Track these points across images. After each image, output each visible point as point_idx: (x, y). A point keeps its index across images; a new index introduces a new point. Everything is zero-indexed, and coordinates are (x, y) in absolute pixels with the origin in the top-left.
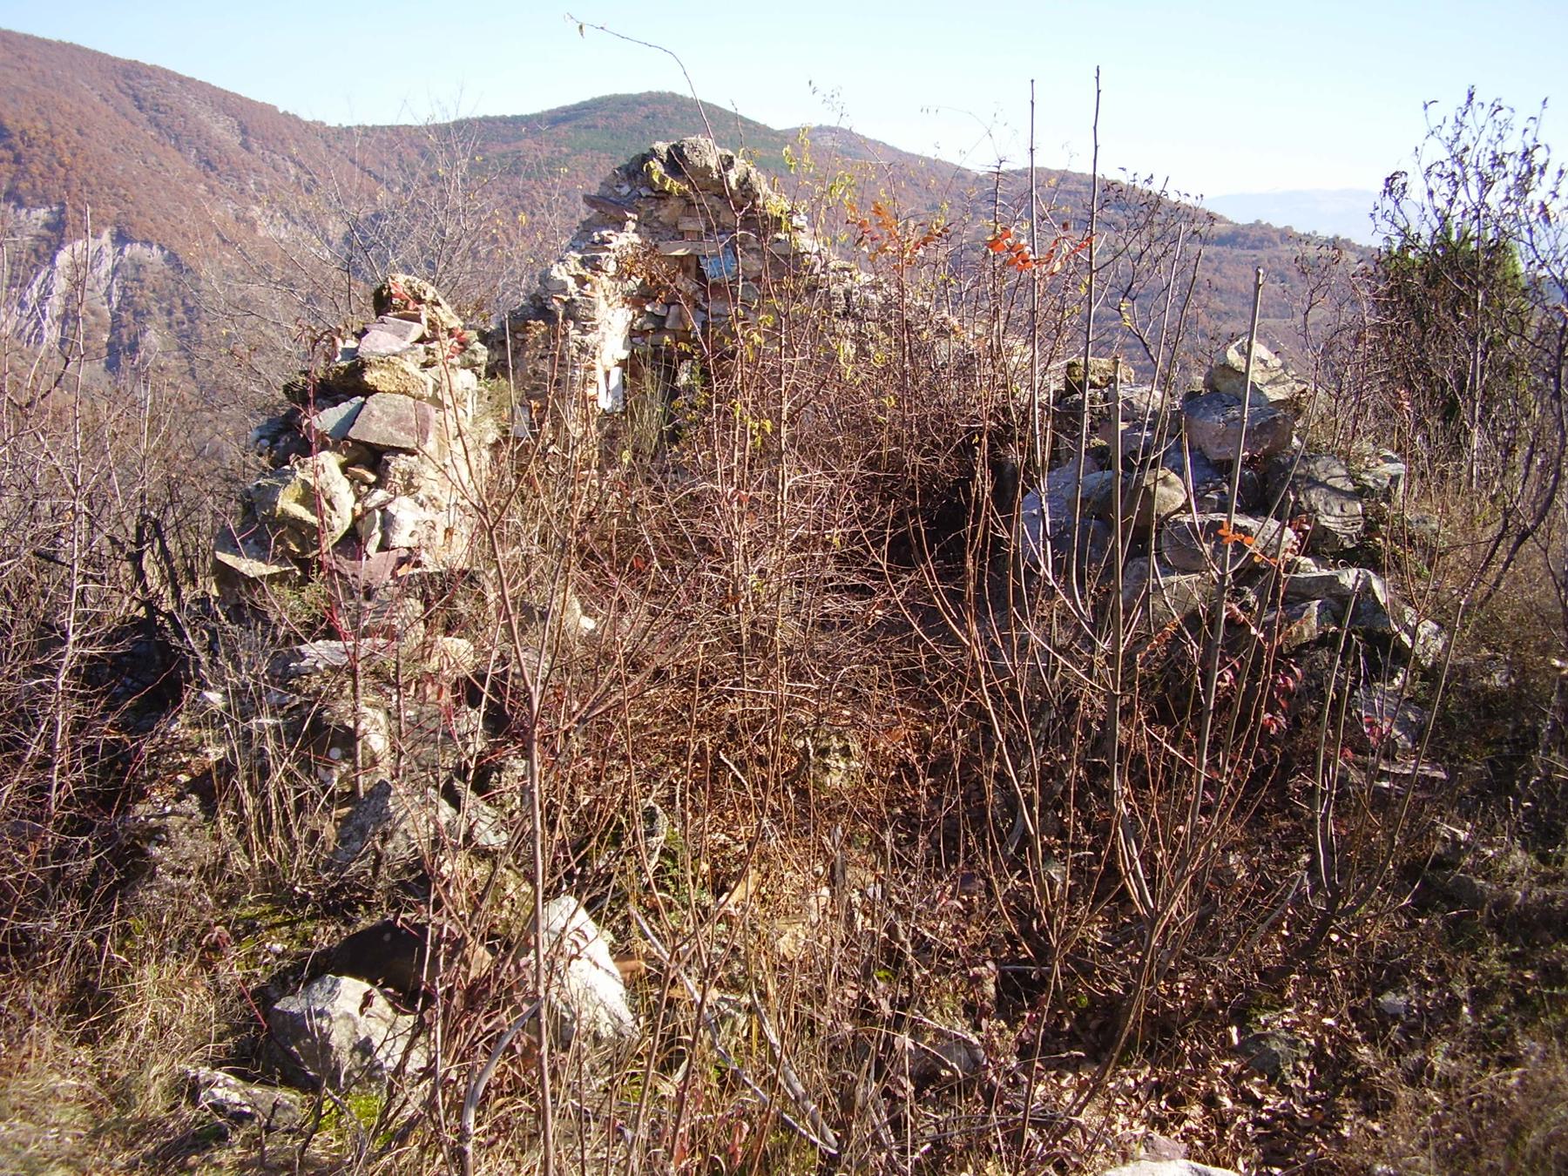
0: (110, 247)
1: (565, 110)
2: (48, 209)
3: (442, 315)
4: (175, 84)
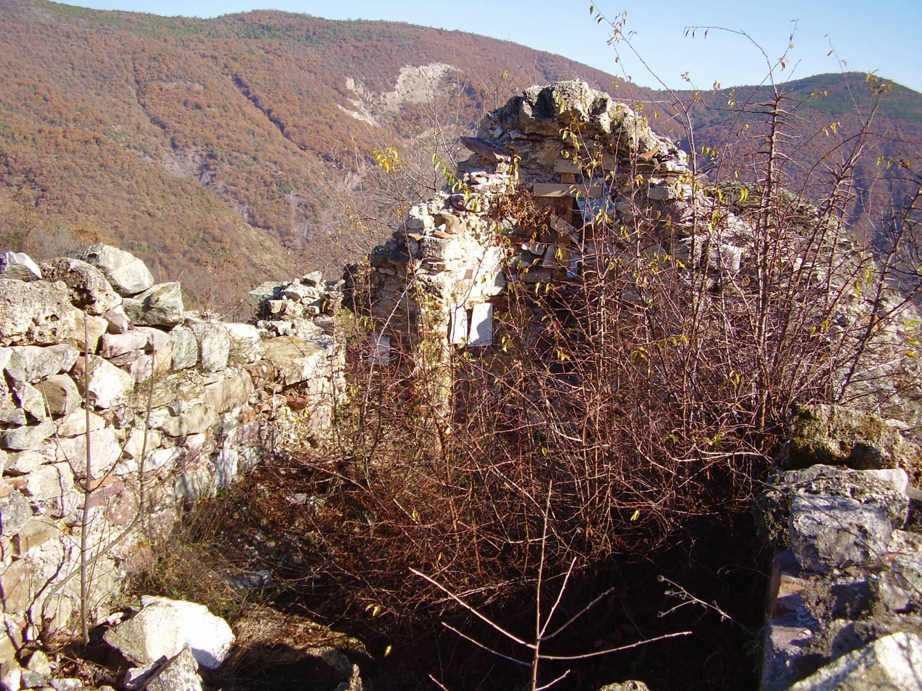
4: (567, 65)
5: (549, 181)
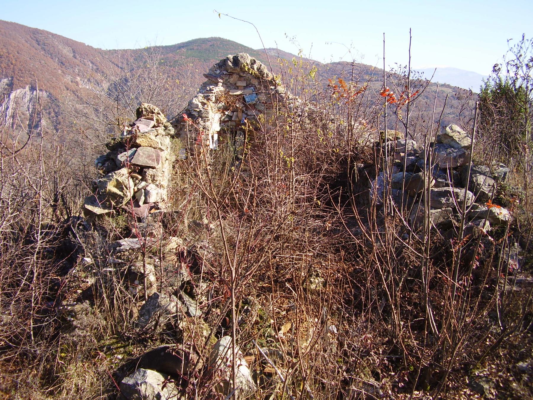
0: (29, 92)
1: (183, 43)
2: (7, 79)
3: (161, 118)
4: (50, 36)
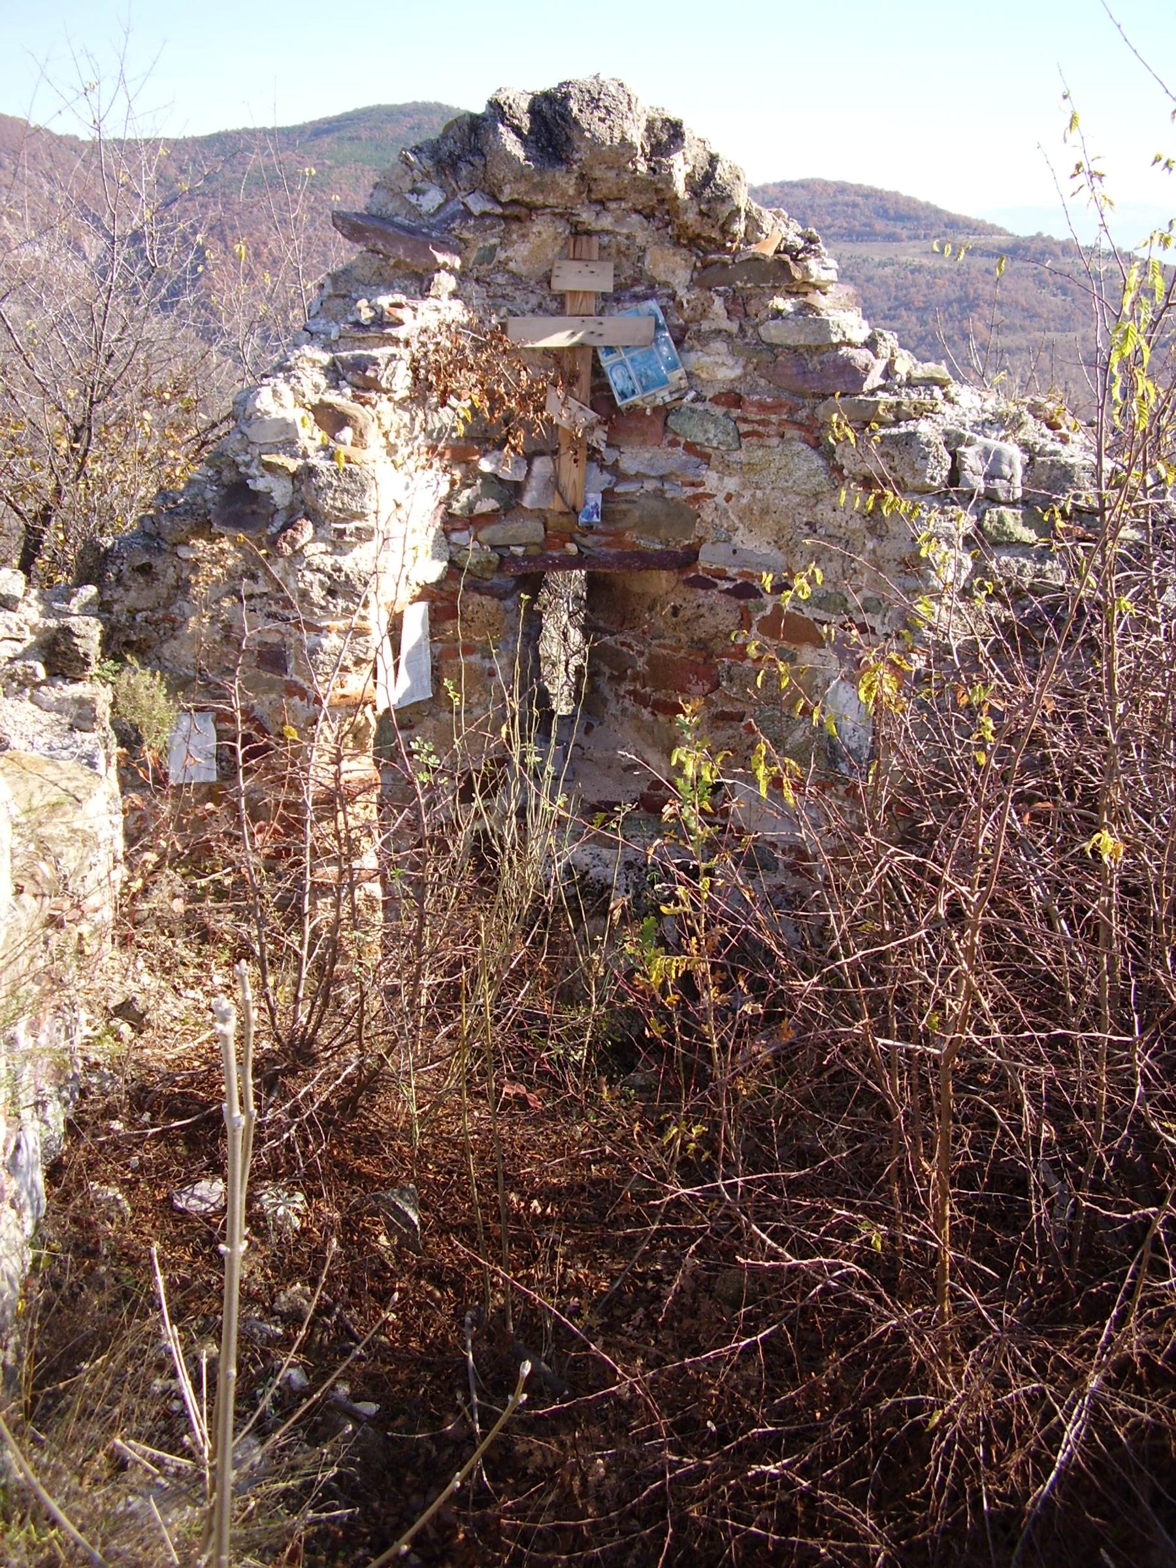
5: (533, 311)
